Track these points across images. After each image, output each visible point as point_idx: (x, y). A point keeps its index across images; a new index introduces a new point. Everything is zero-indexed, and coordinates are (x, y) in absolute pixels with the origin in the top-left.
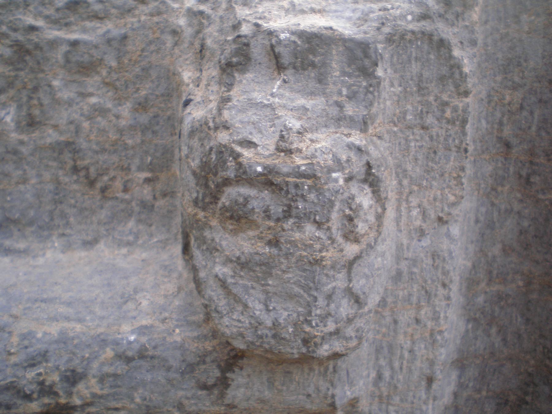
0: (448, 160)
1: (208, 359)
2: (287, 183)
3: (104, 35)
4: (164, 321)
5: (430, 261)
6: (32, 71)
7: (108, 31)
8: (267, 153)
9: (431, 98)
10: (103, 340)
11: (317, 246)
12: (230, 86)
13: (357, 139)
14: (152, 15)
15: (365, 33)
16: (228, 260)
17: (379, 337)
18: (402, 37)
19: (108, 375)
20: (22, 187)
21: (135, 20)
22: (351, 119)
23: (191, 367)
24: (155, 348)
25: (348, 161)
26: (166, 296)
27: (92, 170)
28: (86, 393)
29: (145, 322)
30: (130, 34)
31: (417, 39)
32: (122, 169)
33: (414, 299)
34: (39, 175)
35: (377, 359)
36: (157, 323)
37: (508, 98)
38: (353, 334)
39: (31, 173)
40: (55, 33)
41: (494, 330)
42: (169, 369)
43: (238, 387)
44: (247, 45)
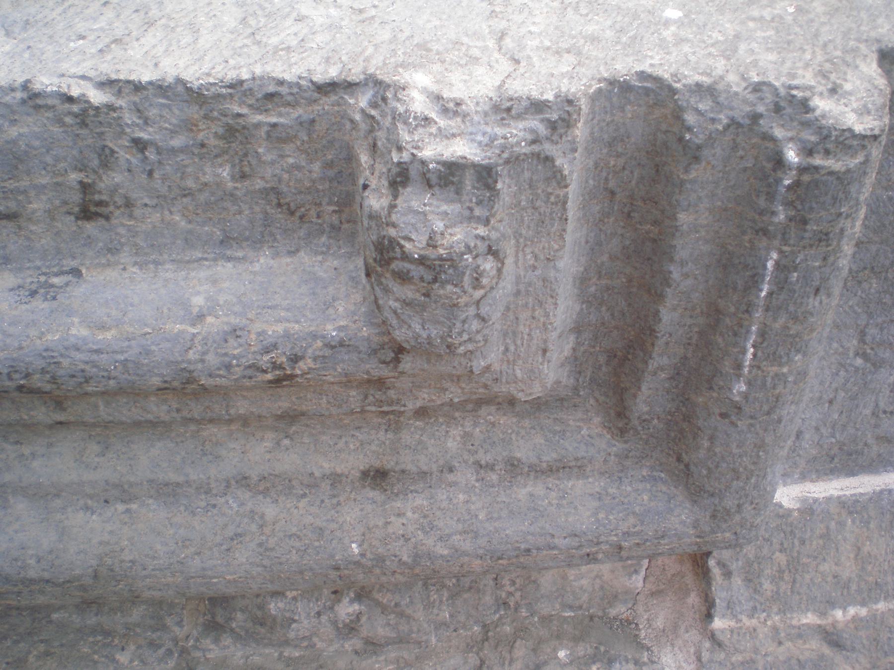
0: (553, 225)
1: (386, 347)
2: (434, 265)
3: (297, 118)
4: (355, 322)
5: (541, 283)
6: (241, 143)
7: (300, 116)
8: (421, 246)
9: (540, 191)
10: (315, 336)
11: (455, 297)
12: (395, 197)
13: (482, 231)
14: (333, 105)
15: (490, 159)
16: (397, 300)
17: (505, 327)
18: (517, 158)
19: (319, 356)
20: (238, 217)
21: (320, 108)
22: (479, 218)
23: (375, 352)
24: (350, 340)
25: (475, 246)
26: (355, 304)
27: (292, 205)
28: (305, 368)
29: (342, 323)
30: (317, 119)
31: (528, 158)
32: (316, 204)
33: (530, 305)
34: (251, 208)
35: (505, 339)
36: (350, 324)
37: (612, 163)
38: (481, 339)
39: (244, 207)
40: (259, 118)
41: (604, 309)
42: (360, 353)
43: (406, 362)
44: (407, 170)
